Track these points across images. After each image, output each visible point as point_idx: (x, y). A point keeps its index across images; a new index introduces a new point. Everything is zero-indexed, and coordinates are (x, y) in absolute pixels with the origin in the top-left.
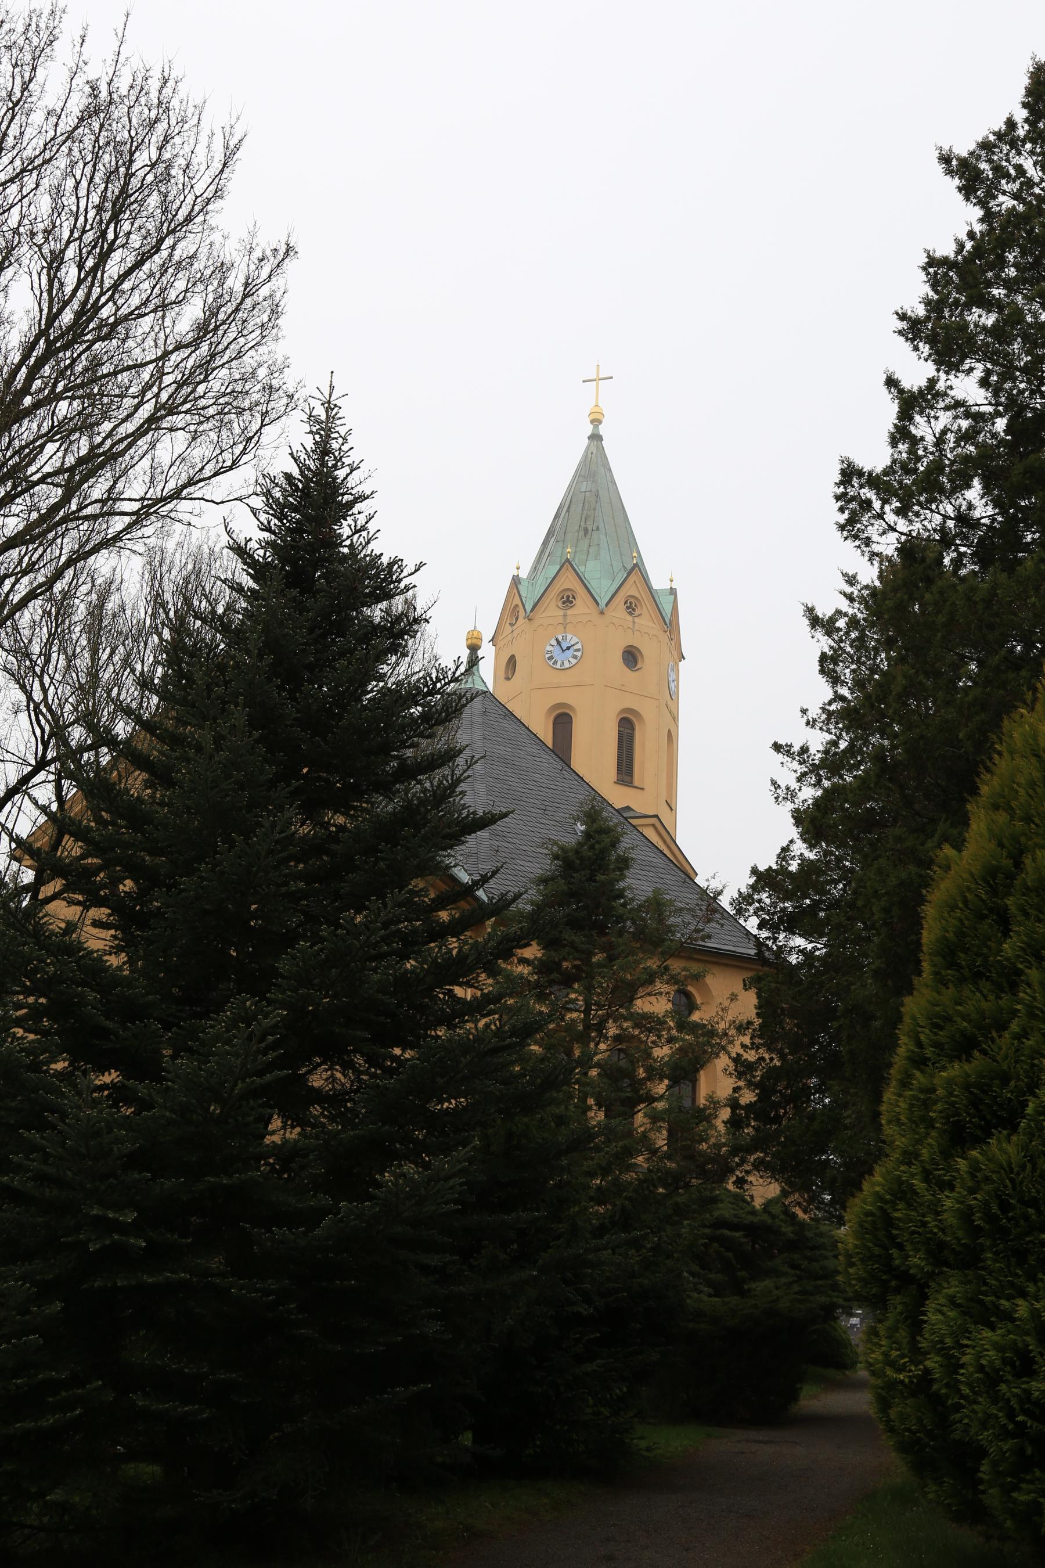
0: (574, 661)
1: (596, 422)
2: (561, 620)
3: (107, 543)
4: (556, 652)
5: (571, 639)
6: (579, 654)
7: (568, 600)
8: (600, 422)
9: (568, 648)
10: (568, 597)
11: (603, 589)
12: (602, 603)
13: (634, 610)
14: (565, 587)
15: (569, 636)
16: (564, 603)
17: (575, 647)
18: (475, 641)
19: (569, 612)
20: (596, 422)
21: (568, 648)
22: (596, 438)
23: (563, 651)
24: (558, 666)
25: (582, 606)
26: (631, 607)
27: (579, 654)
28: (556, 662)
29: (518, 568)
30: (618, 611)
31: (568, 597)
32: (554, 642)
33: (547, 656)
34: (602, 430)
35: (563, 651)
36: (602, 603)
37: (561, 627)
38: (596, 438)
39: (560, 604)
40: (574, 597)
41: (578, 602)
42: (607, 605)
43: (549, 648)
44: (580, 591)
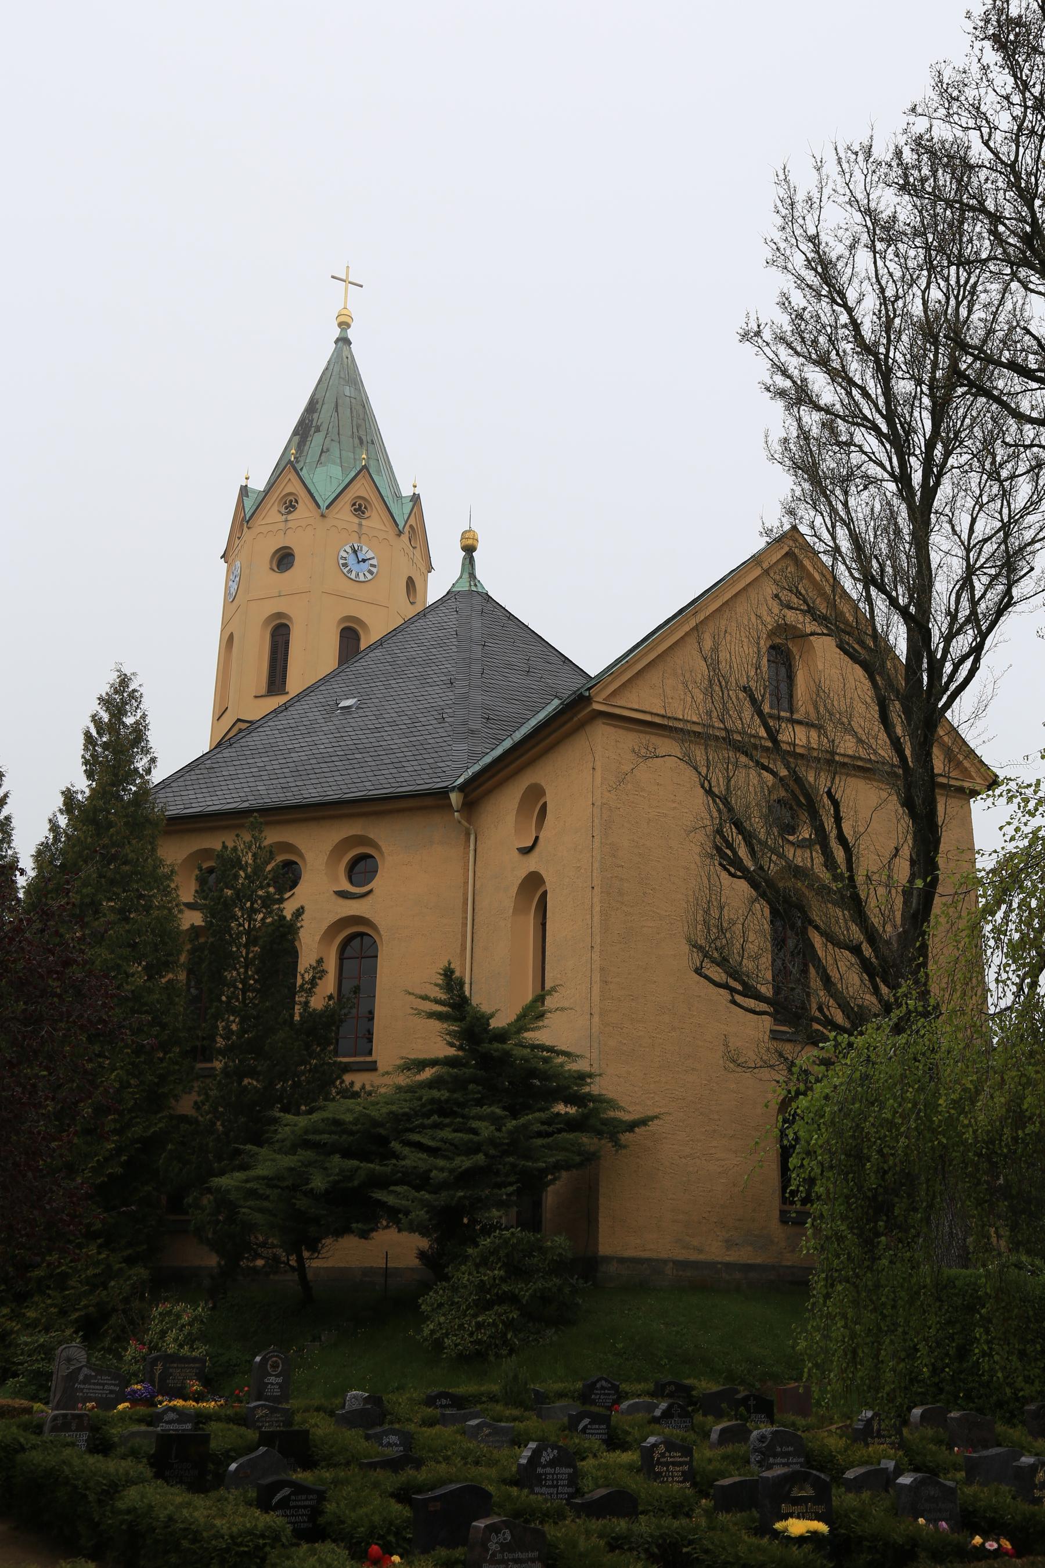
0: (370, 577)
1: (344, 325)
2: (356, 528)
3: (1028, 514)
4: (351, 560)
5: (366, 552)
6: (374, 570)
7: (290, 505)
8: (349, 326)
9: (364, 561)
10: (291, 501)
11: (325, 491)
12: (323, 505)
13: (363, 513)
14: (287, 490)
15: (365, 549)
16: (286, 508)
17: (371, 562)
18: (470, 542)
19: (290, 517)
20: (344, 325)
21: (364, 561)
22: (343, 341)
23: (359, 562)
24: (353, 576)
25: (304, 510)
26: (359, 509)
27: (374, 570)
28: (350, 571)
29: (247, 479)
30: (344, 513)
31: (291, 501)
32: (349, 550)
33: (342, 561)
34: (351, 334)
35: (359, 562)
36: (323, 505)
37: (355, 535)
38: (343, 341)
39: (283, 511)
40: (297, 502)
41: (300, 506)
42: (328, 507)
43: (345, 555)
44: (373, 498)
